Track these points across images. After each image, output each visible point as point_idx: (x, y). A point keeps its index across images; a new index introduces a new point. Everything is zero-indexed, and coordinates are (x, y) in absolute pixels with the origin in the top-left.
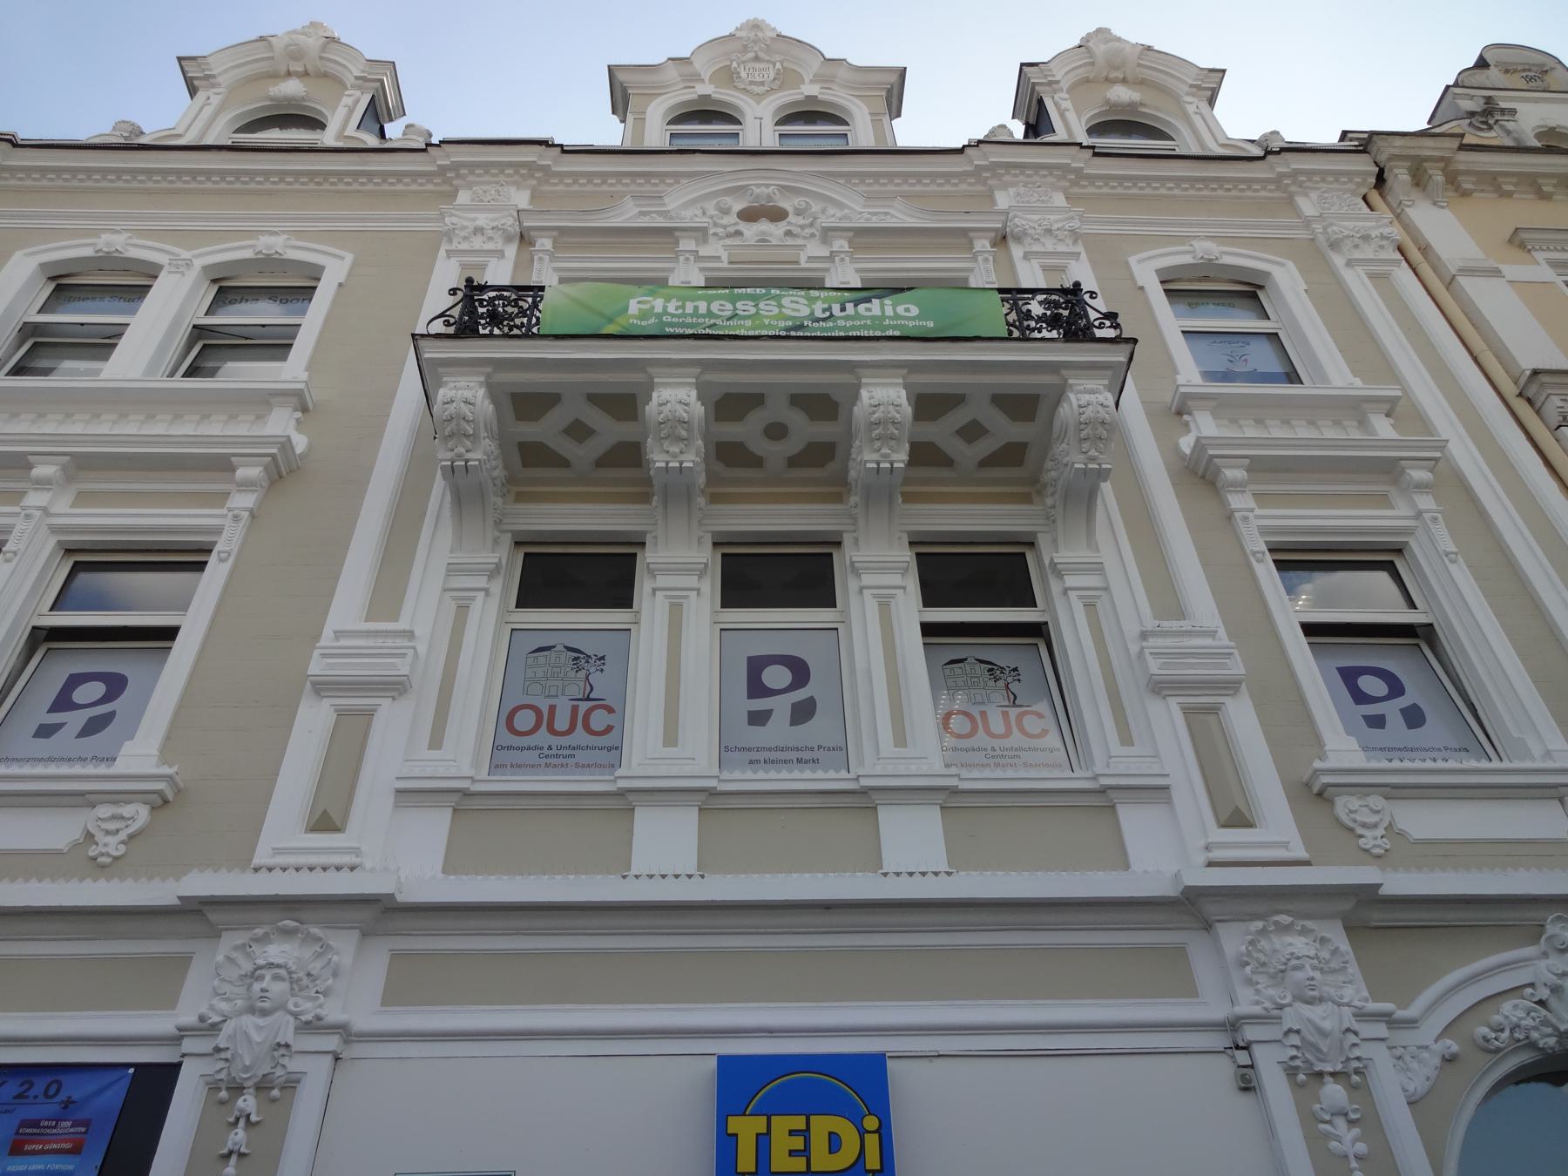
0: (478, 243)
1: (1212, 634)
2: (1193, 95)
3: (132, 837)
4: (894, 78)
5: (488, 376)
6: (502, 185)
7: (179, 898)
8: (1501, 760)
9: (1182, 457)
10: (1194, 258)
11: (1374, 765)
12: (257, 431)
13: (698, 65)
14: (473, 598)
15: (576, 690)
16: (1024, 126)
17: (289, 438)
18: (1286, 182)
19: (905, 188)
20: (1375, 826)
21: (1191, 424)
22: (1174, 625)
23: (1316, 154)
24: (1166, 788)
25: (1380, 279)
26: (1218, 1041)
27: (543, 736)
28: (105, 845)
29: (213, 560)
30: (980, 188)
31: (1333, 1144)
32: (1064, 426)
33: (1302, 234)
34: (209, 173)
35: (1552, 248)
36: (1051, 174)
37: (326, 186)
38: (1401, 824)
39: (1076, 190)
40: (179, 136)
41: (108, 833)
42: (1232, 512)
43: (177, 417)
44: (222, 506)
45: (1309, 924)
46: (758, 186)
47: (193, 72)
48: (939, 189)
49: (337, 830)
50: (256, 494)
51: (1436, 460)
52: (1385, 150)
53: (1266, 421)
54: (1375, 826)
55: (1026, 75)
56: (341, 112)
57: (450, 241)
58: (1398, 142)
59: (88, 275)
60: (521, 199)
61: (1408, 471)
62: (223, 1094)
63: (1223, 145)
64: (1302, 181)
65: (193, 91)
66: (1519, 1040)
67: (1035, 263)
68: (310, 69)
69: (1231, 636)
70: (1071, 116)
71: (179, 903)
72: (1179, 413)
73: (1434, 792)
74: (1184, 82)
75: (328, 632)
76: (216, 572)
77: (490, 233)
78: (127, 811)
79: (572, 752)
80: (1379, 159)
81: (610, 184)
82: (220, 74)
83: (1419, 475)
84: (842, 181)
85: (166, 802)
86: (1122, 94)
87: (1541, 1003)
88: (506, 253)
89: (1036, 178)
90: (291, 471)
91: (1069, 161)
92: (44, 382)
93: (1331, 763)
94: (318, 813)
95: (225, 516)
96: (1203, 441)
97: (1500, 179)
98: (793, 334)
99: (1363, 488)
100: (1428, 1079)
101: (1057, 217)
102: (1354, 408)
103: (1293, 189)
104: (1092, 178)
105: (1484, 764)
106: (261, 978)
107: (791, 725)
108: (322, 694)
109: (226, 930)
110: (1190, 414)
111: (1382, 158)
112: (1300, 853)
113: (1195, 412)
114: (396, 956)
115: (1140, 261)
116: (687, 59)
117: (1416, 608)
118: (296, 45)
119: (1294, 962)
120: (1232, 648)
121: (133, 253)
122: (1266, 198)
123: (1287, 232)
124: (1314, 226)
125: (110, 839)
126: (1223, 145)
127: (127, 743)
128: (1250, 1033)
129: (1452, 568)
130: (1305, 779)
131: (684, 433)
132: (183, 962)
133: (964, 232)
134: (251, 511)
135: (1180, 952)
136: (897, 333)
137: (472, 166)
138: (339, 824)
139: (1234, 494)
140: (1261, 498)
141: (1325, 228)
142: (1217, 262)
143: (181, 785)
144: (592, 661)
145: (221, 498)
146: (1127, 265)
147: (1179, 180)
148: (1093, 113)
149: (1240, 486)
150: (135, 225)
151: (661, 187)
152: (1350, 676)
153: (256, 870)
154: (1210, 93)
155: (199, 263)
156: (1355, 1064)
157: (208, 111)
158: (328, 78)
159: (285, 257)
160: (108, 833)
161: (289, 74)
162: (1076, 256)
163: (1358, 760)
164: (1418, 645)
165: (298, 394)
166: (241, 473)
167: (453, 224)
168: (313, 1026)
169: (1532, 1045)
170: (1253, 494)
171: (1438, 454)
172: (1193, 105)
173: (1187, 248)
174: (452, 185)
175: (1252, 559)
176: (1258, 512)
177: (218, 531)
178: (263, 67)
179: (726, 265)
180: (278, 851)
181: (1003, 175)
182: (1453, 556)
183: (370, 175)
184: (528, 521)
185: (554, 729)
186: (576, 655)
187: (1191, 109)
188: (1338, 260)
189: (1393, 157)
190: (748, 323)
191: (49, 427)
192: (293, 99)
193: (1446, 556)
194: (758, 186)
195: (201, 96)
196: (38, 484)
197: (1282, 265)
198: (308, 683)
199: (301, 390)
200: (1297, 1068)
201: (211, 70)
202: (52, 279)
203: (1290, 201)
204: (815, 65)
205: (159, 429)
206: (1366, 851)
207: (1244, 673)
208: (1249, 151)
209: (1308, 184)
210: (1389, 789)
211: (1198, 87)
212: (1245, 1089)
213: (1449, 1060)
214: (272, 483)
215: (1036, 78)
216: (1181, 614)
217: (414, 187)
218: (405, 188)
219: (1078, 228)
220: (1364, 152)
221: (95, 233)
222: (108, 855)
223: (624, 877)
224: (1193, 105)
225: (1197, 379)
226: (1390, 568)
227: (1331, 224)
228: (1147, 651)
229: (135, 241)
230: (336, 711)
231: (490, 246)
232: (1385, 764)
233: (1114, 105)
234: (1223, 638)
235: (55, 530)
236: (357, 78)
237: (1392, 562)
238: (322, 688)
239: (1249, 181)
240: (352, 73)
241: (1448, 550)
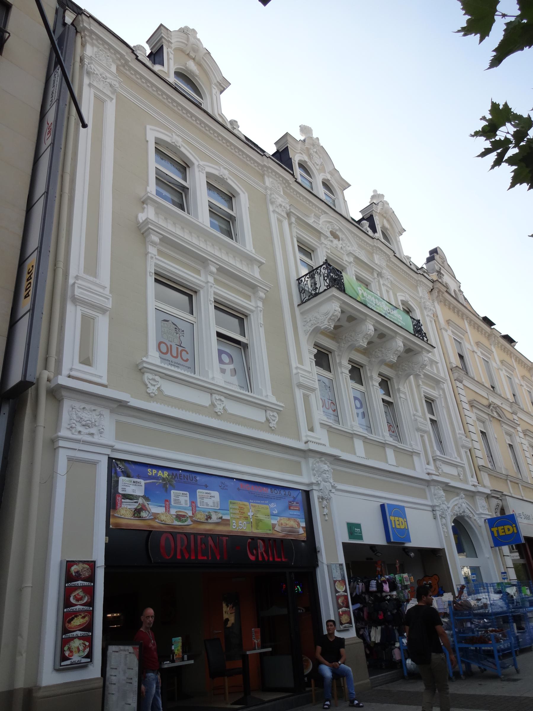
1: (104, 288)
2: (217, 86)
8: (252, 392)
9: (138, 222)
10: (171, 140)
11: (162, 365)
15: (177, 341)
16: (276, 150)
18: (265, 169)
21: (146, 210)
22: (91, 278)
23: (127, 48)
24: (419, 454)
25: (280, 221)
26: (430, 509)
30: (261, 171)
32: (328, 312)
33: (263, 191)
34: (197, 118)
37: (229, 148)
38: (227, 407)
39: (122, 68)
42: (148, 253)
46: (336, 225)
51: (268, 291)
53: (177, 224)
54: (154, 385)
55: (373, 206)
59: (162, 147)
61: (151, 235)
62: (321, 500)
63: (219, 114)
64: (265, 170)
67: (92, 90)
68: (197, 58)
69: (111, 292)
70: (172, 62)
72: (143, 202)
73: (170, 378)
74: (398, 229)
80: (434, 286)
81: (159, 93)
83: (262, 294)
84: (353, 235)
86: (192, 66)
89: (101, 46)
91: (289, 180)
92: (171, 207)
93: (150, 360)
96: (148, 220)
97: (446, 301)
101: (111, 77)
102: (250, 260)
103: (375, 251)
104: (131, 68)
105: (247, 393)
110: (147, 205)
111: (435, 286)
112: (104, 381)
113: (149, 205)
115: (151, 129)
116: (171, 32)
117: (193, 315)
118: (197, 46)
119: (442, 496)
120: (110, 296)
124: (268, 191)
125: (152, 387)
126: (219, 114)
128: (437, 508)
129: (261, 328)
130: (137, 363)
133: (373, 269)
135: (299, 463)
137: (273, 171)
139: (151, 246)
140: (160, 252)
141: (271, 194)
144: (180, 331)
146: (145, 128)
148: (181, 67)
149: (155, 244)
152: (220, 352)
158: (322, 169)
160: (152, 385)
162: (111, 99)
163: (158, 362)
164: (241, 349)
170: (158, 249)
171: (268, 290)
172: (215, 90)
173: (170, 135)
175: (148, 274)
176: (157, 257)
182: (151, 274)
185: (166, 352)
186: (176, 327)
187: (214, 91)
188: (271, 208)
191: (217, 253)
192: (193, 73)
193: (210, 301)
197: (244, 193)
203: (262, 176)
204: (331, 168)
206: (217, 413)
207: (111, 307)
208: (227, 125)
209: (270, 174)
210: (164, 375)
211: (220, 84)
212: (434, 518)
215: (164, 35)
216: (95, 275)
217: (253, 165)
219: (117, 88)
220: (433, 282)
224: (215, 90)
225: (154, 193)
226: (190, 297)
227: (273, 194)
228: (76, 285)
234: (107, 292)
237: (192, 296)
241: (261, 322)
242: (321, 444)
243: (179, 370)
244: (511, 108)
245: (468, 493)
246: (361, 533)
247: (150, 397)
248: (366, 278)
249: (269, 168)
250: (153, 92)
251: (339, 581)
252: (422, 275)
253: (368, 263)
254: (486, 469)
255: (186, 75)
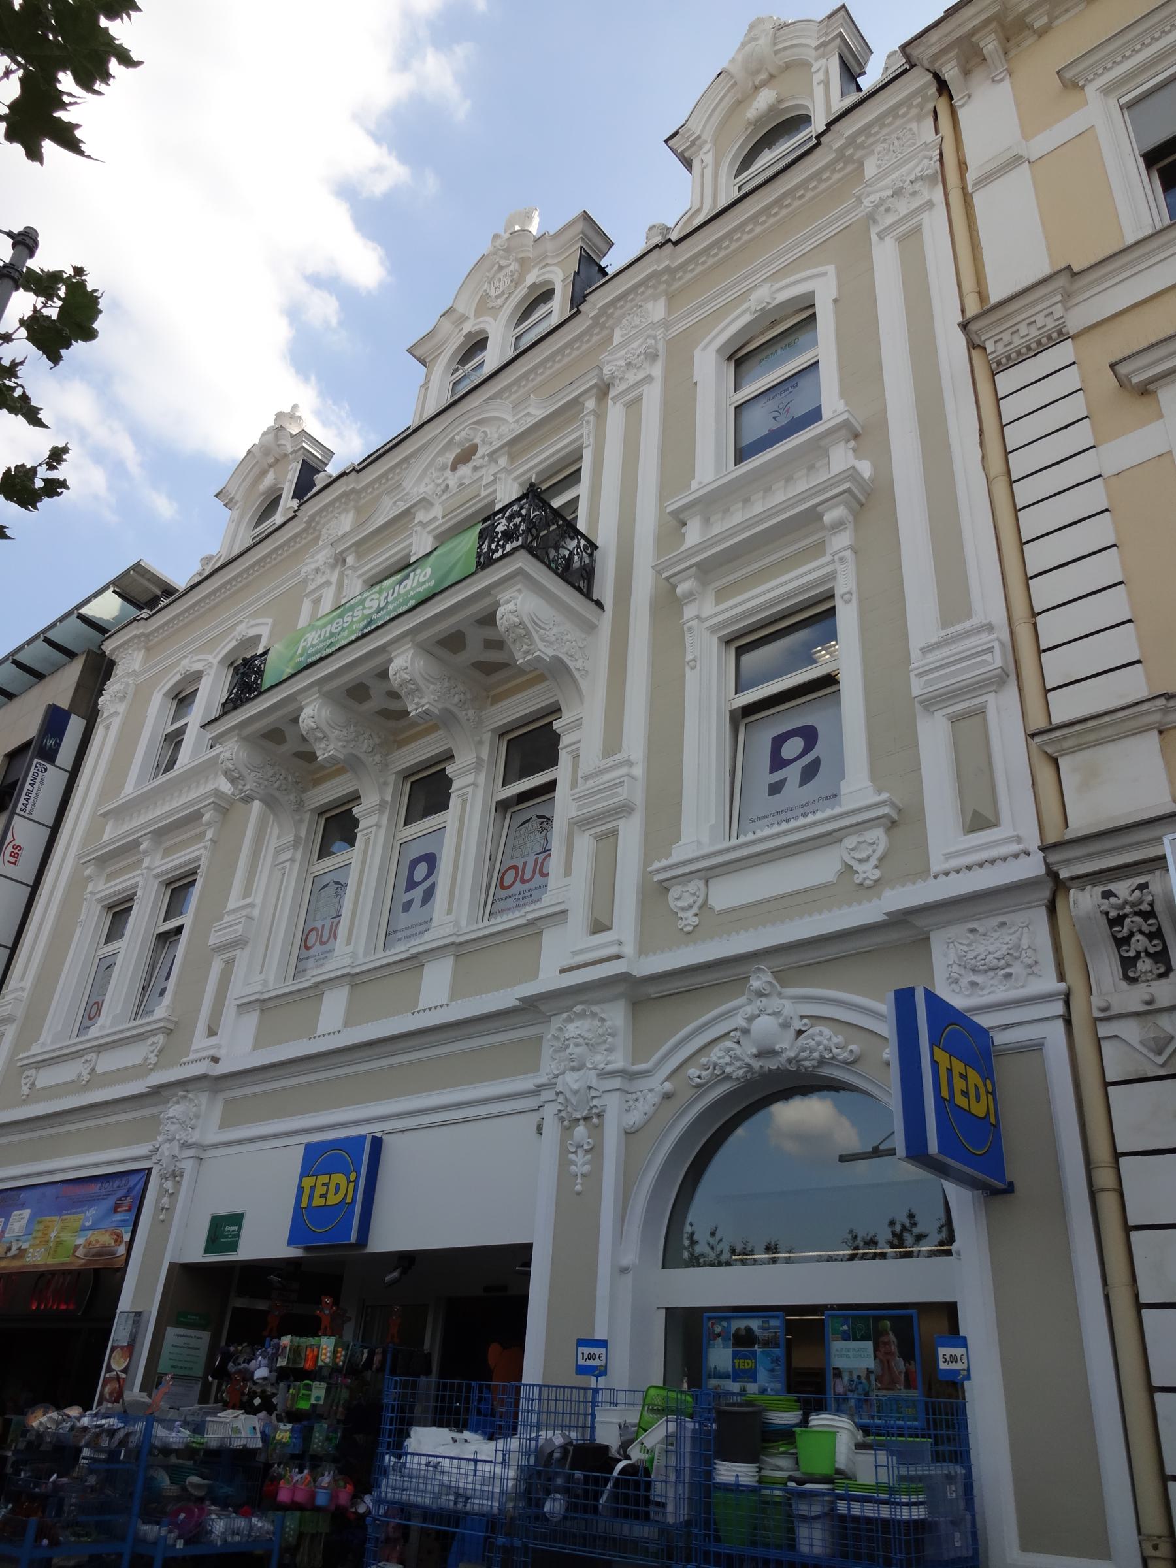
0: (903, 207)
3: (881, 859)
4: (580, 226)
5: (319, 691)
6: (640, 306)
7: (519, 999)
12: (821, 477)
13: (461, 308)
14: (467, 794)
17: (853, 468)
19: (531, 385)
20: (690, 907)
27: (518, 887)
28: (865, 872)
29: (838, 603)
31: (573, 1167)
35: (1127, 54)
36: (647, 287)
40: (699, 211)
41: (860, 861)
43: (789, 479)
44: (823, 554)
45: (595, 1009)
46: (458, 434)
47: (680, 147)
48: (716, 259)
49: (995, 825)
50: (848, 532)
52: (921, 53)
56: (819, 91)
57: (875, 221)
58: (934, 36)
60: (657, 310)
65: (688, 164)
66: (718, 1076)
71: (886, 918)
75: (915, 653)
76: (847, 618)
77: (911, 189)
78: (155, 1039)
79: (530, 893)
82: (702, 131)
85: (894, 822)
87: (800, 1032)
88: (935, 200)
90: (868, 495)
94: (968, 818)
95: (833, 562)
98: (365, 631)
99: (773, 557)
100: (645, 1114)
103: (859, 154)
106: (567, 1047)
107: (769, 795)
108: (932, 709)
109: (932, 930)
114: (228, 1101)
121: (782, 297)
122: (840, 180)
123: (750, 281)
127: (843, 783)
131: (413, 687)
132: (539, 1039)
134: (851, 547)
136: (412, 603)
138: (992, 818)
142: (770, 306)
143: (901, 805)
145: (819, 548)
147: (754, 218)
150: (192, 648)
151: (397, 478)
153: (935, 877)
154: (838, 40)
155: (215, 661)
156: (595, 1110)
157: (709, 172)
159: (192, 670)
160: (860, 861)
161: (756, 88)
165: (846, 424)
166: (828, 518)
167: (872, 202)
168: (185, 1145)
169: (728, 1077)
174: (607, 328)
177: (832, 576)
178: (256, 470)
179: (441, 521)
180: (948, 856)
181: (613, 313)
183: (281, 547)
184: (501, 717)
189: (935, 57)
190: (345, 633)
194: (458, 434)
195: (696, 165)
196: (833, 529)
198: (917, 706)
199: (847, 419)
200: (563, 1117)
201: (694, 133)
202: (729, 359)
205: (758, 508)
206: (861, 884)
211: (824, 44)
213: (667, 1096)
214: (856, 515)
218: (588, 345)
221: (744, 297)
222: (689, 925)
223: (413, 1013)
229: (253, 622)
230: (949, 719)
231: (917, 202)
232: (776, 829)
233: (757, 121)
235: (157, 876)
236: (817, 48)
238: (931, 703)
239: (817, 175)
240: (808, 46)
242: (958, 871)
243: (819, 816)
244: (108, 84)
245: (780, 962)
246: (238, 1236)
247: (26, 1101)
248: (387, 559)
249: (852, 140)
250: (818, 190)
251: (122, 1348)
252: (835, 128)
253: (552, 410)
254: (1106, 725)
255: (777, 122)
